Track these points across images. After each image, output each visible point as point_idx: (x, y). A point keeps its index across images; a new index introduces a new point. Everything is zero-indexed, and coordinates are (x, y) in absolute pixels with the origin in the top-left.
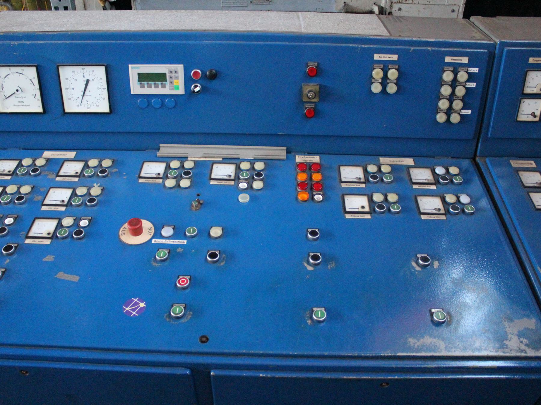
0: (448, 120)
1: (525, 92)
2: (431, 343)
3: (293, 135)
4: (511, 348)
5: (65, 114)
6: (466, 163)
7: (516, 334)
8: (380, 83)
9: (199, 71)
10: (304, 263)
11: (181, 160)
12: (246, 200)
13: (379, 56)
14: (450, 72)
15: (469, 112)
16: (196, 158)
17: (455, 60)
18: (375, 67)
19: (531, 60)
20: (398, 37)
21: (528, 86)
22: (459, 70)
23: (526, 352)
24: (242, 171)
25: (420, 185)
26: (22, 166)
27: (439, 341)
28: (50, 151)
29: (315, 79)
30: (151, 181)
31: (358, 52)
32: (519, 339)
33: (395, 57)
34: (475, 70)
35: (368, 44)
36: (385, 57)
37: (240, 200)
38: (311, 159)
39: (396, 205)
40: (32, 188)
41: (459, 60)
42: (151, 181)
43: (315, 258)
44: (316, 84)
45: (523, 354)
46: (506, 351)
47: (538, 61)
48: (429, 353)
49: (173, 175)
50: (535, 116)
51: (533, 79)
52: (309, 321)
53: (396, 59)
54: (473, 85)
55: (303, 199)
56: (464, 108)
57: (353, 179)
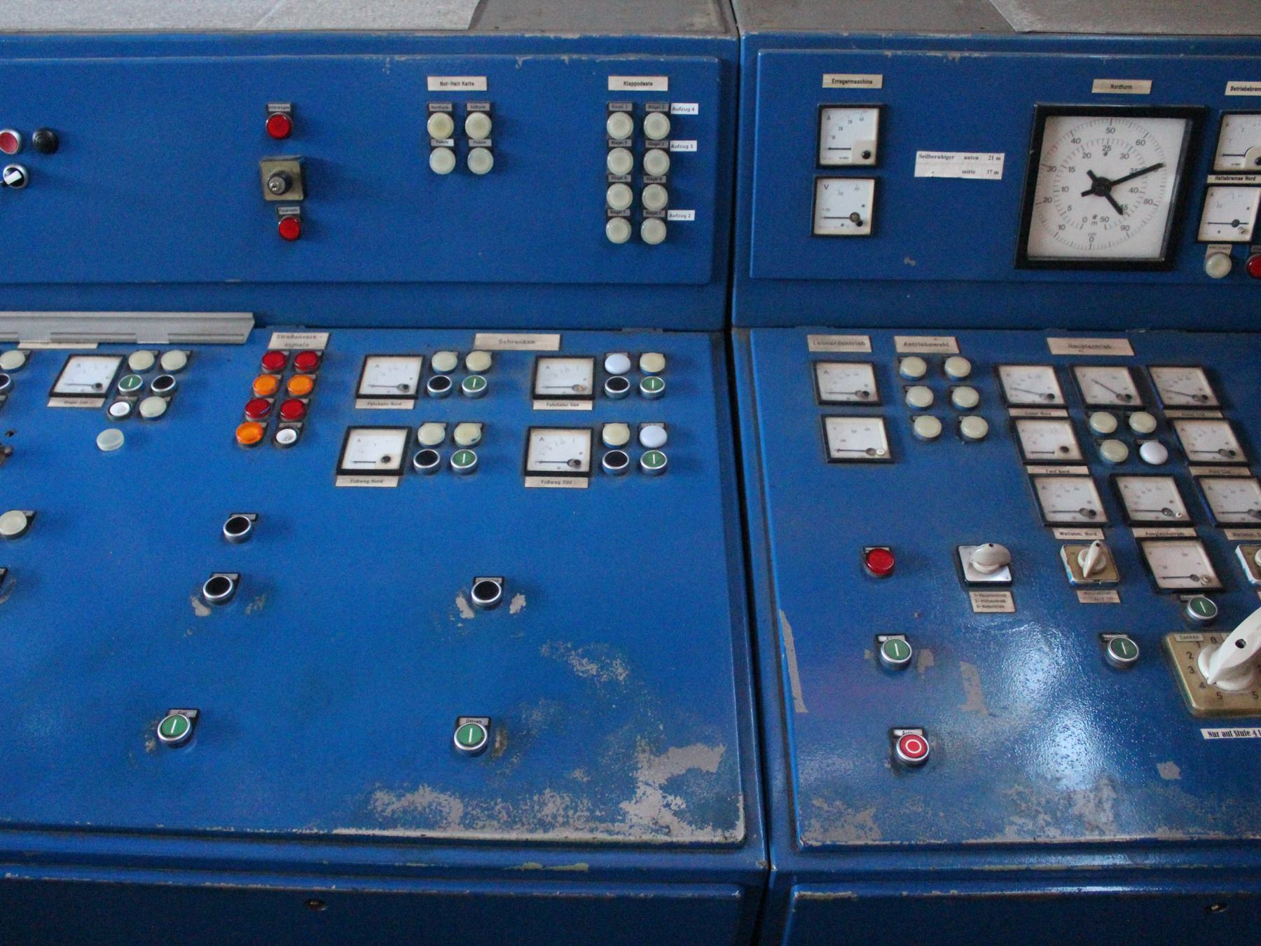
0: (636, 235)
1: (824, 162)
2: (430, 805)
4: (635, 820)
6: (700, 346)
7: (660, 785)
8: (449, 148)
9: (15, 134)
10: (193, 599)
11: (159, 349)
12: (116, 443)
13: (439, 82)
14: (623, 114)
15: (688, 215)
16: (37, 343)
17: (635, 84)
18: (433, 110)
19: (828, 81)
20: (492, 30)
21: (832, 147)
22: (647, 109)
23: (668, 834)
24: (646, 376)
25: (551, 402)
26: (129, 370)
27: (451, 799)
29: (290, 143)
30: (79, 403)
31: (385, 72)
32: (664, 797)
33: (876, 81)
35: (1125, 52)
36: (455, 84)
37: (101, 446)
38: (308, 341)
39: (655, 453)
41: (644, 84)
42: (79, 403)
43: (218, 586)
44: (292, 157)
45: (662, 838)
46: (617, 830)
47: (847, 82)
48: (415, 830)
50: (860, 224)
51: (841, 129)
52: (150, 743)
53: (484, 88)
54: (690, 146)
55: (249, 441)
56: (674, 203)
57: (390, 389)
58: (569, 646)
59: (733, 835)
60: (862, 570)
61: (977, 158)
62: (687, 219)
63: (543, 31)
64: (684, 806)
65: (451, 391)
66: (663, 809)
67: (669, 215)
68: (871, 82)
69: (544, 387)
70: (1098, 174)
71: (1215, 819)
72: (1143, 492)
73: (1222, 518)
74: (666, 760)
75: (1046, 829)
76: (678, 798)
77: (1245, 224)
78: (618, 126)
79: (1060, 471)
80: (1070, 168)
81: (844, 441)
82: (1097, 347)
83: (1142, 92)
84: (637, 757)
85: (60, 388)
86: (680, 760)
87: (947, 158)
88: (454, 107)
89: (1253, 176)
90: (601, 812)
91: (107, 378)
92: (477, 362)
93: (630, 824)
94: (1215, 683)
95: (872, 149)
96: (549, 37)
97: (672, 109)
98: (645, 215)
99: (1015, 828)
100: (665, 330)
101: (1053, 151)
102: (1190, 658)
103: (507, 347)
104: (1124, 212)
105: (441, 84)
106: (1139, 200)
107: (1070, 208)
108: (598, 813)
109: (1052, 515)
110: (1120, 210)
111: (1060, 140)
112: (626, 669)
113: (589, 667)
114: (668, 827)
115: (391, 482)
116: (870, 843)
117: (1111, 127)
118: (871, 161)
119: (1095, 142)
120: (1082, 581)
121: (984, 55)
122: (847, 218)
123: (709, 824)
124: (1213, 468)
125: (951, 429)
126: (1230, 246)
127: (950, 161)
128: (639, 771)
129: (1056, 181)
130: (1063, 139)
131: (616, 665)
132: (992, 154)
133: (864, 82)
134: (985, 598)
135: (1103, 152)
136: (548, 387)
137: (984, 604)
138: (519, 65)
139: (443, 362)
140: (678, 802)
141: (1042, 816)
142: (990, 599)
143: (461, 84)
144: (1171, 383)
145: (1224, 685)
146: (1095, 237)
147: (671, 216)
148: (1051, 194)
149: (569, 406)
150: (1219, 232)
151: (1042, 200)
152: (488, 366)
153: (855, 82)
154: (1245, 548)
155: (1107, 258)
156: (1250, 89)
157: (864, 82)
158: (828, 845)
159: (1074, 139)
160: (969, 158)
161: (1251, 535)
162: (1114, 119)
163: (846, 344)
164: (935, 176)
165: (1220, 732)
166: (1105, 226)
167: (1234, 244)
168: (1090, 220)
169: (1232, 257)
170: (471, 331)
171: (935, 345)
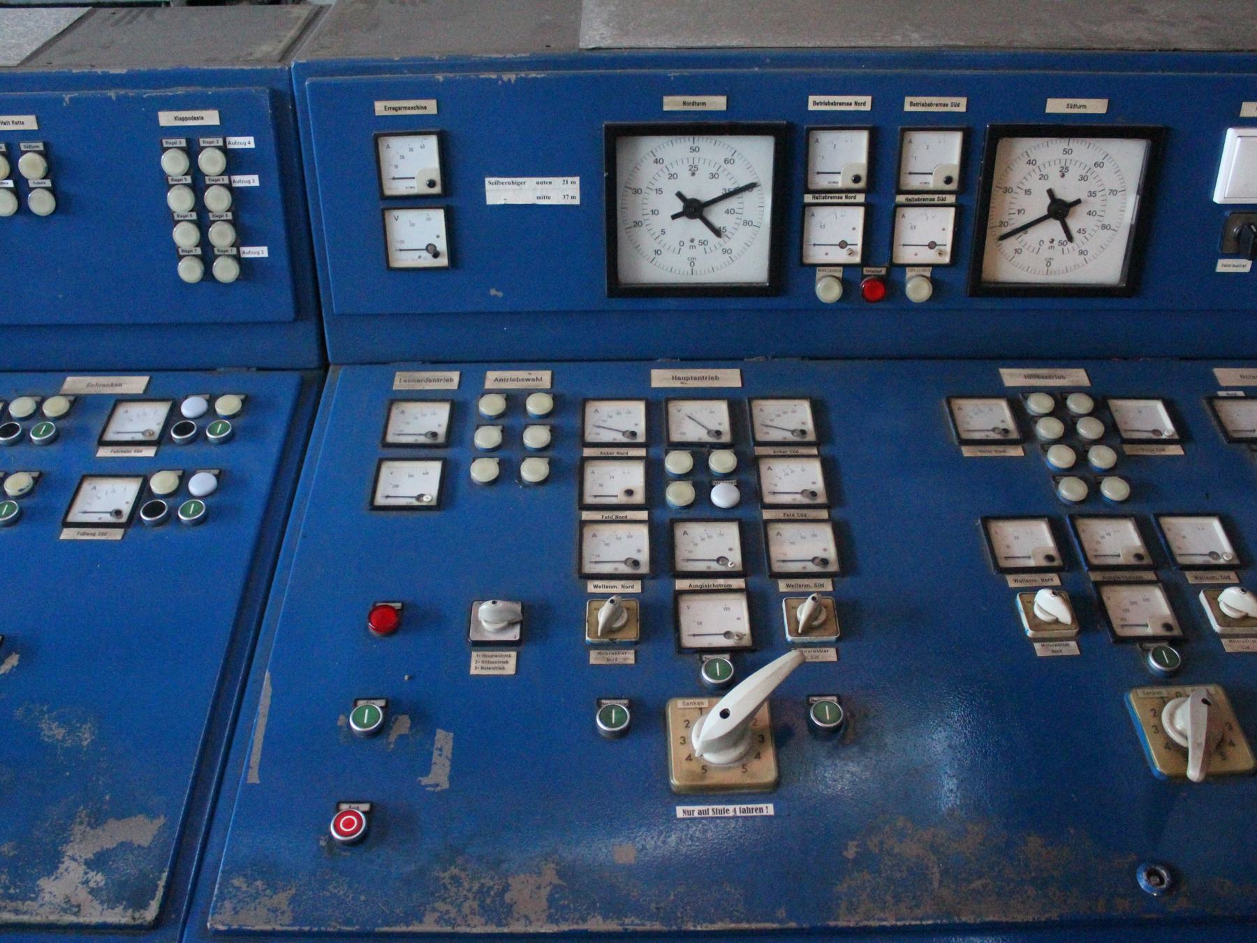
1: (388, 192)
3: (111, 325)
5: (390, 269)
15: (261, 252)
19: (380, 108)
22: (202, 144)
25: (116, 448)
28: (140, 375)
33: (431, 107)
34: (245, 142)
36: (5, 124)
39: (195, 502)
40: (36, 480)
47: (400, 108)
49: (220, 433)
50: (436, 255)
54: (252, 180)
58: (45, 709)
59: (142, 916)
60: (367, 628)
61: (550, 183)
62: (261, 256)
63: (92, 66)
64: (102, 884)
65: (196, 435)
66: (80, 886)
67: (241, 252)
68: (425, 108)
69: (114, 433)
70: (689, 196)
71: (658, 909)
72: (703, 539)
73: (1182, 560)
74: (101, 833)
75: (469, 916)
76: (100, 874)
78: (173, 163)
81: (397, 486)
82: (703, 378)
83: (718, 109)
84: (73, 829)
85: (110, 436)
86: (113, 834)
87: (518, 184)
88: (45, 145)
89: (853, 195)
90: (15, 889)
91: (158, 424)
92: (55, 406)
93: (41, 902)
94: (702, 756)
95: (863, 173)
96: (96, 72)
97: (227, 143)
98: (216, 253)
99: (437, 915)
100: (259, 369)
102: (687, 726)
103: (93, 391)
104: (723, 234)
107: (663, 232)
108: (12, 891)
109: (593, 565)
110: (717, 232)
111: (1015, 160)
112: (93, 734)
113: (56, 732)
114: (79, 906)
115: (117, 534)
116: (278, 928)
117: (695, 146)
118: (437, 190)
119: (1052, 163)
120: (596, 641)
123: (121, 904)
124: (788, 511)
125: (509, 471)
126: (841, 268)
127: (522, 186)
128: (71, 844)
129: (1011, 203)
130: (644, 160)
131: (85, 729)
132: (565, 178)
133: (418, 108)
134: (487, 659)
135: (690, 172)
136: (119, 433)
137: (483, 665)
138: (66, 102)
139: (191, 407)
140: (98, 878)
141: (467, 904)
142: (492, 660)
143: (11, 123)
144: (773, 417)
145: (710, 758)
146: (1052, 262)
147: (244, 252)
149: (133, 453)
150: (916, 254)
151: (998, 224)
152: (65, 411)
153: (409, 108)
154: (1024, 596)
155: (752, 283)
156: (834, 104)
157: (418, 108)
158: (235, 929)
159: (657, 159)
160: (542, 183)
161: (808, 586)
162: (696, 137)
164: (507, 203)
165: (696, 810)
166: (1063, 249)
167: (845, 266)
168: (688, 244)
169: (844, 282)
170: (54, 375)
171: (528, 380)
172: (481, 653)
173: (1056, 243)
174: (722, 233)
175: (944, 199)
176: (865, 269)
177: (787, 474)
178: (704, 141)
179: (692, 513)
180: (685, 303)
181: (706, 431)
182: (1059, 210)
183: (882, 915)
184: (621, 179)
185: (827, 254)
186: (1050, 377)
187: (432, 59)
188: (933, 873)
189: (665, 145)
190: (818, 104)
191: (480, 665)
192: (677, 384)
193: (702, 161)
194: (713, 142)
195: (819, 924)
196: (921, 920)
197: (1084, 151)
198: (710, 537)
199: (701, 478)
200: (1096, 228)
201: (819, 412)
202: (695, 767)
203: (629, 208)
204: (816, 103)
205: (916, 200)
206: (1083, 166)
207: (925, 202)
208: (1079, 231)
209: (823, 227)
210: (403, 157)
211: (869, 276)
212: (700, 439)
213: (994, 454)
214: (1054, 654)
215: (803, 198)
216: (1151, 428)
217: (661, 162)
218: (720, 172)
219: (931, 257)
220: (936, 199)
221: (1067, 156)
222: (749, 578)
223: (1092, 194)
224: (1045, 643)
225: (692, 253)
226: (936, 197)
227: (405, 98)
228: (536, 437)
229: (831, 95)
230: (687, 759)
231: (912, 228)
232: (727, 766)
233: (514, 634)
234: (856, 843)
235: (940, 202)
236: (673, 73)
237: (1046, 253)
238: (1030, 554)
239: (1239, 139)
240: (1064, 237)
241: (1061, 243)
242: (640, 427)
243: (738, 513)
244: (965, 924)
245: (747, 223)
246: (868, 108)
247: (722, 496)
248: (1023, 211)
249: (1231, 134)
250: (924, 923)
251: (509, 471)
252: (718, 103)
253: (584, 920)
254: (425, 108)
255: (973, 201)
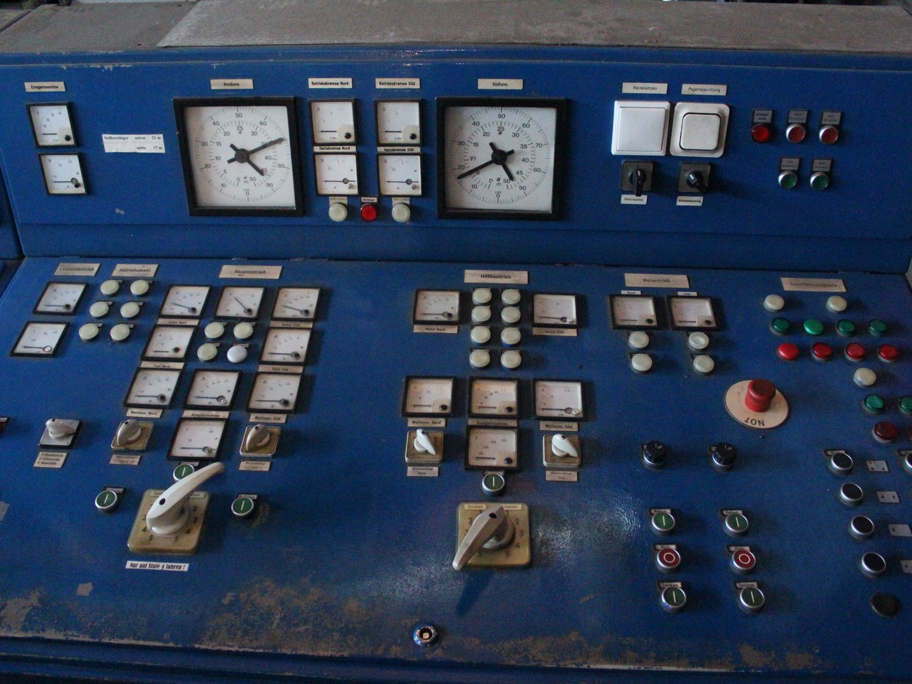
1: (41, 144)
19: (29, 87)
33: (61, 86)
61: (144, 138)
68: (57, 87)
70: (239, 147)
77: (416, 182)
79: (163, 366)
80: (217, 143)
82: (256, 272)
87: (124, 139)
89: (348, 147)
95: (352, 131)
101: (202, 131)
105: (634, 88)
106: (274, 165)
107: (225, 171)
109: (258, 403)
110: (261, 172)
117: (239, 113)
118: (72, 142)
119: (491, 124)
120: (117, 448)
121: (129, 65)
122: (69, 182)
124: (276, 367)
125: (104, 333)
132: (154, 135)
133: (52, 87)
142: (50, 457)
148: (209, 162)
153: (47, 87)
157: (52, 87)
159: (475, 122)
160: (138, 138)
163: (82, 269)
166: (254, 183)
167: (349, 196)
168: (242, 180)
171: (141, 271)
172: (45, 453)
173: (501, 181)
174: (264, 173)
175: (413, 150)
176: (362, 198)
177: (286, 341)
178: (245, 110)
179: (213, 366)
180: (270, 221)
181: (244, 309)
182: (501, 157)
183: (231, 644)
184: (193, 135)
185: (335, 188)
186: (500, 277)
187: (61, 54)
188: (276, 619)
189: (219, 112)
190: (315, 84)
191: (42, 461)
192: (236, 276)
193: (507, 124)
194: (251, 110)
195: (188, 645)
196: (255, 649)
197: (514, 116)
198: (219, 382)
199: (225, 341)
200: (530, 171)
201: (716, 307)
202: (146, 536)
203: (199, 158)
204: (313, 83)
205: (392, 150)
206: (514, 126)
207: (399, 152)
208: (518, 173)
209: (330, 169)
210: (48, 120)
211: (366, 203)
212: (238, 314)
213: (436, 331)
214: (420, 475)
215: (313, 149)
216: (561, 316)
217: (218, 124)
218: (258, 131)
219: (408, 190)
220: (407, 150)
221: (239, 119)
222: (233, 412)
223: (524, 146)
224: (416, 467)
225: (246, 186)
226: (406, 148)
227: (45, 81)
228: (129, 310)
229: (333, 77)
230: (142, 530)
231: (392, 170)
232: (166, 536)
233: (66, 442)
234: (233, 594)
235: (409, 152)
236: (215, 64)
237: (495, 188)
238: (431, 404)
239: (621, 108)
240: (507, 177)
241: (505, 181)
242: (455, 311)
243: (518, 374)
244: (285, 654)
245: (280, 166)
246: (350, 86)
247: (234, 354)
248: (474, 158)
249: (617, 105)
250: (257, 651)
251: (104, 333)
252: (247, 84)
253: (43, 631)
254: (57, 87)
255: (433, 152)
